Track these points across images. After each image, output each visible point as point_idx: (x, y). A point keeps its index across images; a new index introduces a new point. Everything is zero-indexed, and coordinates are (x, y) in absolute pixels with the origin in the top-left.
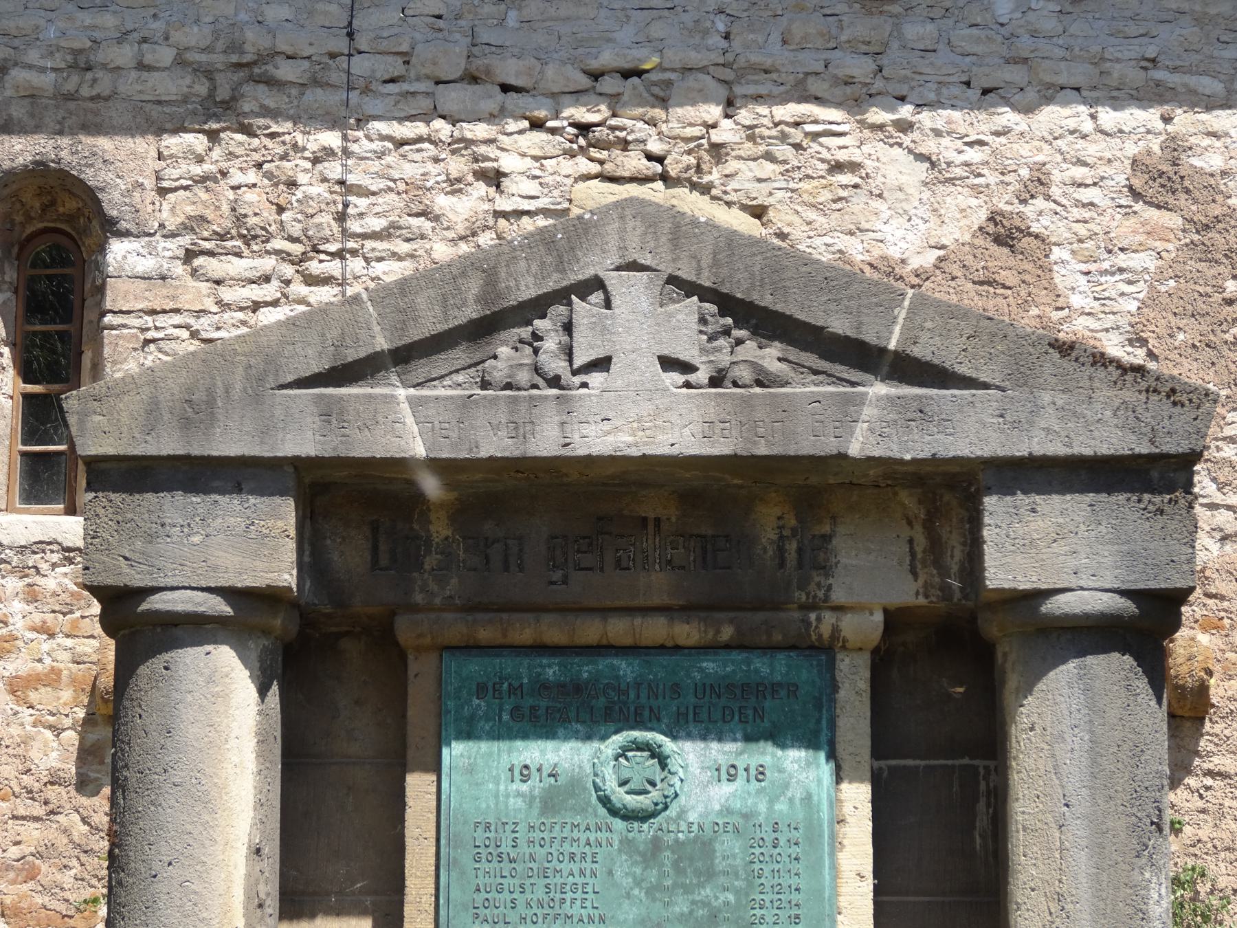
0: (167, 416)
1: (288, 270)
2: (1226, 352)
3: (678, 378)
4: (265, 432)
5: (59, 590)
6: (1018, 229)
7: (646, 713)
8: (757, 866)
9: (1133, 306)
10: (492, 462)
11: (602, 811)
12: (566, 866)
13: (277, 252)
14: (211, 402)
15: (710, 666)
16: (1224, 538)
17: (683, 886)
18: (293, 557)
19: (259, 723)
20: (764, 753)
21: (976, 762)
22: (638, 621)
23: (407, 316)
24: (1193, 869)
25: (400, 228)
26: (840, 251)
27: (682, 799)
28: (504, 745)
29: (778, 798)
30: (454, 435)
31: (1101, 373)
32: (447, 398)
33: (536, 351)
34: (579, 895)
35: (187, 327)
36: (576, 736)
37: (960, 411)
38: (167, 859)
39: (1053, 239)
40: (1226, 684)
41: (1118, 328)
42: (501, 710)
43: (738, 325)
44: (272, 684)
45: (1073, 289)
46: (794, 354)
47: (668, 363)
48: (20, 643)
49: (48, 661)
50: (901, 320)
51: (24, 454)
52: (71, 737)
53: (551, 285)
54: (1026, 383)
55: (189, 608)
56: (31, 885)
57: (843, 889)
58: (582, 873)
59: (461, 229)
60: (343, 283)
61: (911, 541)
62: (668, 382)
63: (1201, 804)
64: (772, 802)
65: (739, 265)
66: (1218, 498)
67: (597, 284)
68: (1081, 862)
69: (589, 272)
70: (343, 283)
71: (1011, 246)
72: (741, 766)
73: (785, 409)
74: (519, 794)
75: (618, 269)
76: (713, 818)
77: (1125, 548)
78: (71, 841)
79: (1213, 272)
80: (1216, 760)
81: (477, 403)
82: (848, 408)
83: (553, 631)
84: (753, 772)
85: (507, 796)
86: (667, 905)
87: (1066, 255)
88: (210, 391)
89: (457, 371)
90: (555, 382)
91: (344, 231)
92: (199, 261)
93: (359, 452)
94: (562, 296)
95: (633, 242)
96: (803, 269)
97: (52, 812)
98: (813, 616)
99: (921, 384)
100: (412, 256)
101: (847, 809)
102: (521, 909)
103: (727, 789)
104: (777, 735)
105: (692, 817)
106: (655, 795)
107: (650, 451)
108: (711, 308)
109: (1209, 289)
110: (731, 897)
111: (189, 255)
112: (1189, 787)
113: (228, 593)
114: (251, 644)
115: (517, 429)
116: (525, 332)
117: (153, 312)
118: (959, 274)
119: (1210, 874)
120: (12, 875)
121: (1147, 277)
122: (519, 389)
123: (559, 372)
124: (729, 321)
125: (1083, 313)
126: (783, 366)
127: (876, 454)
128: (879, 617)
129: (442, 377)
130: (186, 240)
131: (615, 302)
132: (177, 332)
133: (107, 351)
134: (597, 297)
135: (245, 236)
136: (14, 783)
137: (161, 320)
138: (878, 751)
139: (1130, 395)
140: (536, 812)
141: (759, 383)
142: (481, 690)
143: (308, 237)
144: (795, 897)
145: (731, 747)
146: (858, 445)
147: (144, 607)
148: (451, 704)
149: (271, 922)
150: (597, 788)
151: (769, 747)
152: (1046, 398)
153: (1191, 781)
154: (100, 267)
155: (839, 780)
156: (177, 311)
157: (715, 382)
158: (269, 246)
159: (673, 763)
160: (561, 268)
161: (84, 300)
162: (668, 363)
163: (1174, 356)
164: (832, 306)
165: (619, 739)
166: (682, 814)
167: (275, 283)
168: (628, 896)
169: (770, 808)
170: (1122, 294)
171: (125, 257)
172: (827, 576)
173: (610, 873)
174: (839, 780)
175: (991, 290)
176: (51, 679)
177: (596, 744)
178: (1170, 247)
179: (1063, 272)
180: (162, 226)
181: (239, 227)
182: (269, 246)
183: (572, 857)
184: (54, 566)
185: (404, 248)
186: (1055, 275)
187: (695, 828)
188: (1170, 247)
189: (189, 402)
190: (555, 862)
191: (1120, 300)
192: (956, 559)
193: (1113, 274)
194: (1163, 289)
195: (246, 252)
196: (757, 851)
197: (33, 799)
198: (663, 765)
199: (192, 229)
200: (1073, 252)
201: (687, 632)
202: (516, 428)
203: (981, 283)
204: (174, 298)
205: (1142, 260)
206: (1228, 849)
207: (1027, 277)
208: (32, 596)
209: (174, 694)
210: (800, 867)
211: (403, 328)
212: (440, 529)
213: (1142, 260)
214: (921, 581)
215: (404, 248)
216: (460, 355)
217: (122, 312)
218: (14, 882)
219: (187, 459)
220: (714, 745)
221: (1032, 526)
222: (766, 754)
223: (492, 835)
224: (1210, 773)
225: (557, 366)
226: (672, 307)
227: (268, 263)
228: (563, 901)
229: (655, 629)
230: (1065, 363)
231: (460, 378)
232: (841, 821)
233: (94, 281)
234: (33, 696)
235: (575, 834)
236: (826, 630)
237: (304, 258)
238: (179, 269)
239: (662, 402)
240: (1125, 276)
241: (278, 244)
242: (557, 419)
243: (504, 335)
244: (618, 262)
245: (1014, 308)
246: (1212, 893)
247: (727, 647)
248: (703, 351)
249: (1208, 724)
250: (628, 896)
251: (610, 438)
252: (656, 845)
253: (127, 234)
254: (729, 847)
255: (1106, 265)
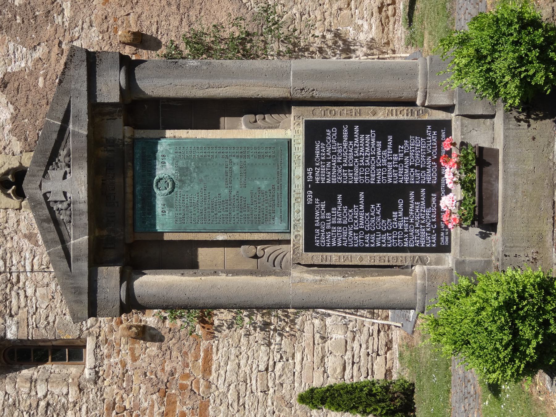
0: (78, 298)
1: (15, 288)
2: (38, 23)
3: (68, 175)
4: (82, 274)
5: (108, 349)
6: (2, 81)
7: (149, 183)
8: (185, 157)
9: (25, 49)
10: (89, 220)
11: (173, 193)
12: (186, 202)
13: (10, 291)
14: (75, 288)
15: (138, 168)
16: (91, 26)
17: (190, 174)
18: (112, 267)
19: (152, 275)
20: (159, 155)
21: (160, 104)
22: (127, 185)
23: (53, 241)
24: (183, 38)
25: (3, 256)
26: (9, 132)
27: (170, 174)
28: (157, 217)
29: (169, 152)
30: (83, 229)
31: (67, 73)
32: (73, 231)
33: (62, 209)
34: (192, 199)
35: (32, 316)
36: (155, 199)
37: (76, 107)
38: (184, 295)
39: (5, 71)
40: (132, 27)
41: (31, 54)
42: (148, 218)
43: (55, 161)
44: (126, 301)
45: (20, 66)
46: (62, 147)
47: (65, 177)
48: (122, 359)
49: (127, 351)
50: (54, 121)
51: (69, 361)
52: (148, 344)
53: (45, 206)
54: (69, 91)
55: (125, 291)
56: (189, 353)
57: (191, 137)
58: (187, 198)
59: (3, 239)
60: (19, 272)
61: (107, 119)
62: (69, 178)
63: (166, 35)
64: (170, 153)
65: (40, 160)
66: (80, 27)
67: (45, 195)
68: (184, 81)
69: (42, 197)
70: (19, 272)
71: (7, 83)
72: (162, 161)
73: (76, 149)
74: (169, 213)
75: (41, 190)
76: (174, 167)
77: (109, 69)
78: (177, 343)
79: (14, 26)
80: (153, 31)
81: (74, 224)
82: (75, 134)
83: (130, 205)
84: (163, 158)
85: (169, 216)
86: (194, 178)
87: (10, 68)
88: (72, 288)
89: (67, 229)
90: (69, 205)
91: (4, 272)
92: (13, 313)
93: (87, 252)
94: (48, 203)
95: (34, 186)
96: (41, 145)
97: (169, 348)
98: (126, 143)
99: (70, 117)
100: (11, 253)
101: (172, 135)
102: (196, 212)
103: (167, 164)
104: (155, 152)
105: (174, 172)
106: (169, 181)
107: (86, 182)
108: (51, 167)
109: (19, 27)
110: (193, 163)
111: (11, 316)
112: (161, 38)
113: (121, 283)
114: (133, 277)
115: (81, 214)
116: (57, 212)
117: (28, 326)
118: (15, 98)
119: (185, 33)
120: (186, 359)
121: (16, 45)
122: (71, 214)
123: (67, 204)
124: (54, 163)
125: (27, 63)
126: (65, 150)
127: (87, 128)
128: (126, 127)
129: (68, 232)
130: (7, 317)
131: (49, 190)
132: (34, 319)
133: (39, 338)
134: (48, 195)
135: (6, 300)
136: (161, 359)
137: (30, 323)
138: (157, 128)
139: (72, 66)
140: (173, 209)
141: (69, 156)
142: (144, 222)
143: (6, 282)
144: (193, 148)
145: (157, 163)
146: (84, 132)
147: (125, 302)
148: (147, 229)
149: (199, 271)
150: (167, 195)
151: (157, 154)
152: (73, 86)
153: (159, 37)
154: (14, 341)
155: (165, 137)
156: (28, 319)
157: (69, 166)
158: (9, 293)
159: (161, 176)
160: (40, 204)
161: (24, 346)
162: (65, 177)
163: (39, 38)
164: (50, 138)
165: (155, 190)
166: (173, 174)
167: (19, 291)
168: (192, 187)
169: (172, 154)
170: (21, 52)
171: (12, 334)
172: (116, 140)
173: (187, 191)
174: (165, 137)
175: (20, 89)
176: (132, 350)
177: (157, 195)
178: (7, 38)
179: (15, 68)
180: (3, 324)
181: (3, 302)
182: (9, 293)
183: (183, 200)
184: (101, 351)
185: (9, 255)
186: (15, 71)
187: (176, 172)
188: (7, 38)
189: (75, 293)
190: (185, 205)
191: (23, 53)
192: (111, 108)
193: (15, 54)
194: (19, 40)
195: (10, 300)
196: (182, 157)
197: (165, 354)
198: (162, 179)
199: (4, 315)
200: (9, 66)
201: (130, 173)
202: (81, 214)
203: (18, 92)
204: (24, 320)
205: (11, 46)
206: (178, 28)
207: (16, 79)
208: (109, 356)
209: (146, 295)
210: (186, 147)
211: (56, 242)
212: (105, 233)
213: (11, 46)
214: (116, 117)
215: (9, 255)
216: (63, 228)
217: (28, 334)
218: (188, 358)
219: (89, 293)
220: (157, 167)
221: (104, 90)
222: (159, 155)
223: (178, 219)
224: (157, 32)
225: (65, 205)
226: (50, 176)
227: (13, 293)
228: (193, 200)
229: (129, 181)
230: (64, 82)
231: (68, 228)
232: (175, 137)
233: (18, 343)
234: (137, 355)
235: (178, 200)
236: (129, 140)
237: (12, 283)
238: (15, 319)
239: (74, 179)
240: (16, 51)
241: (8, 291)
242: (78, 204)
243: (58, 217)
244: (39, 190)
245: (25, 83)
246: (190, 33)
247: (133, 164)
248: (61, 169)
249: (143, 32)
250: (192, 187)
251: (83, 191)
252: (180, 181)
253: (5, 334)
254: (181, 164)
255: (13, 56)
